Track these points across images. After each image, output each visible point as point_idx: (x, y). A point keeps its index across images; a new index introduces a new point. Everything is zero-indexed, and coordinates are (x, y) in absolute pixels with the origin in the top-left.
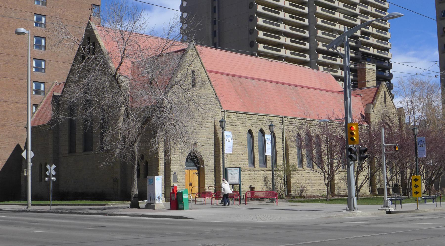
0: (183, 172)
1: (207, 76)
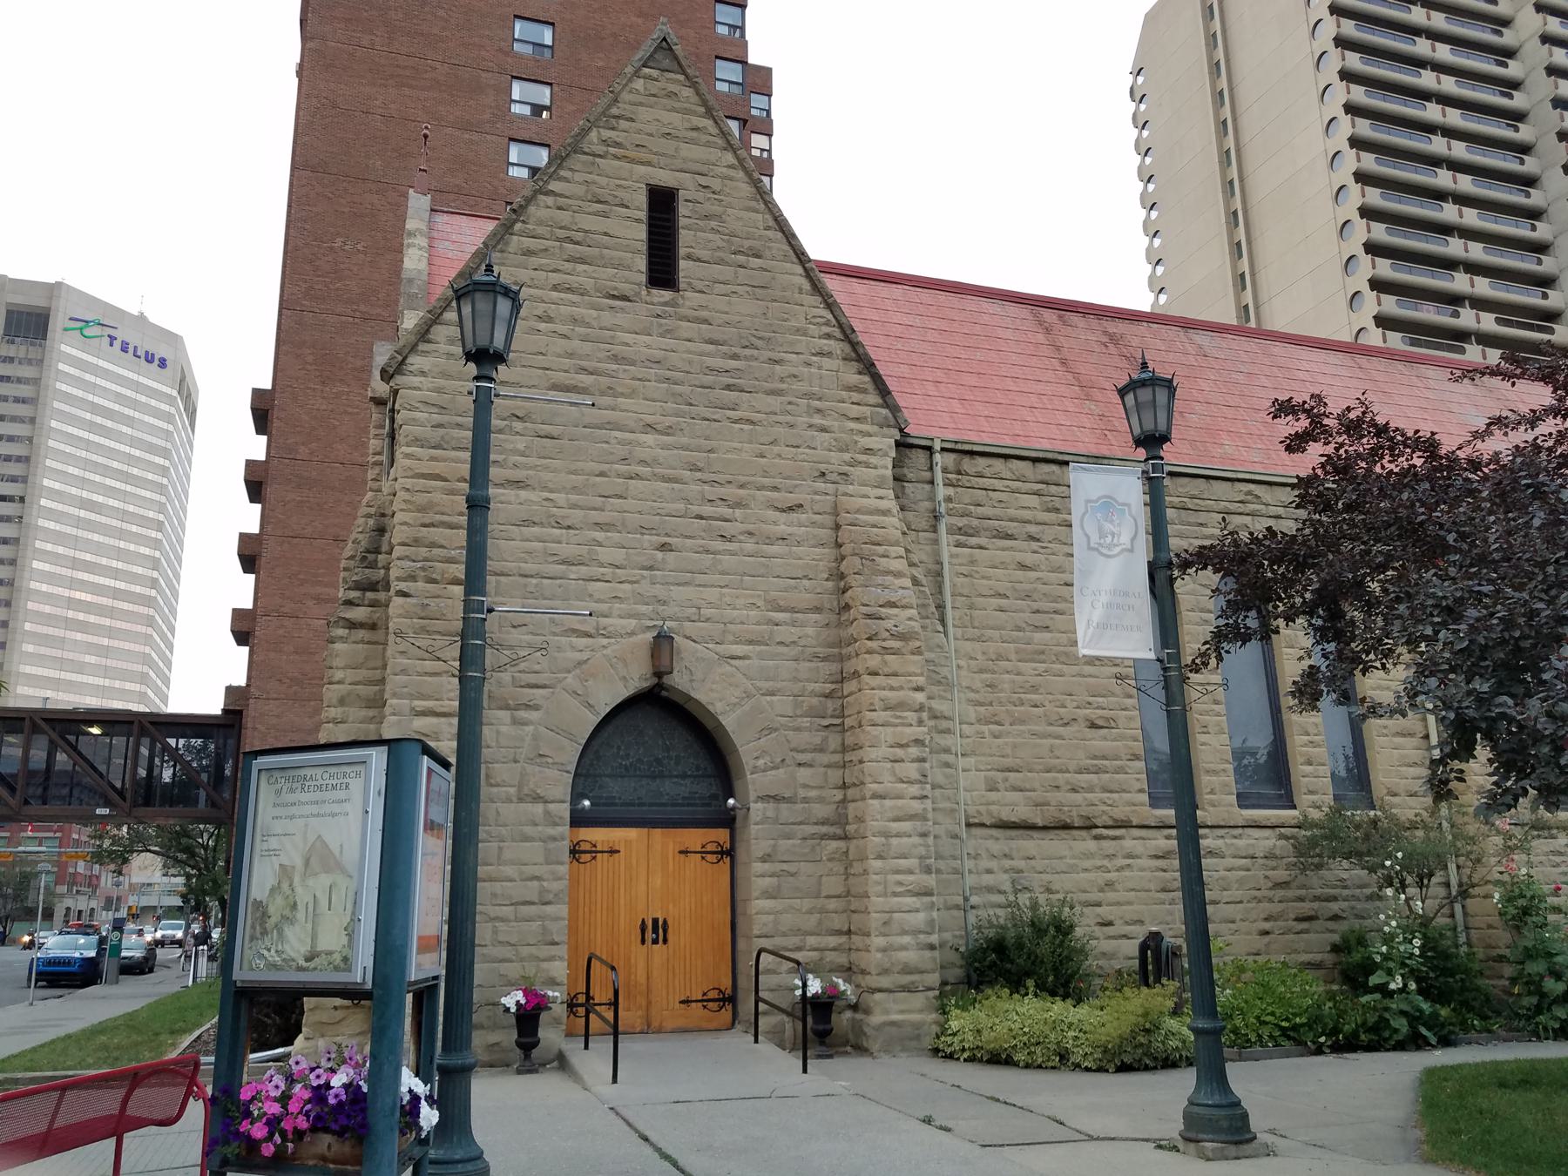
1: (771, 223)
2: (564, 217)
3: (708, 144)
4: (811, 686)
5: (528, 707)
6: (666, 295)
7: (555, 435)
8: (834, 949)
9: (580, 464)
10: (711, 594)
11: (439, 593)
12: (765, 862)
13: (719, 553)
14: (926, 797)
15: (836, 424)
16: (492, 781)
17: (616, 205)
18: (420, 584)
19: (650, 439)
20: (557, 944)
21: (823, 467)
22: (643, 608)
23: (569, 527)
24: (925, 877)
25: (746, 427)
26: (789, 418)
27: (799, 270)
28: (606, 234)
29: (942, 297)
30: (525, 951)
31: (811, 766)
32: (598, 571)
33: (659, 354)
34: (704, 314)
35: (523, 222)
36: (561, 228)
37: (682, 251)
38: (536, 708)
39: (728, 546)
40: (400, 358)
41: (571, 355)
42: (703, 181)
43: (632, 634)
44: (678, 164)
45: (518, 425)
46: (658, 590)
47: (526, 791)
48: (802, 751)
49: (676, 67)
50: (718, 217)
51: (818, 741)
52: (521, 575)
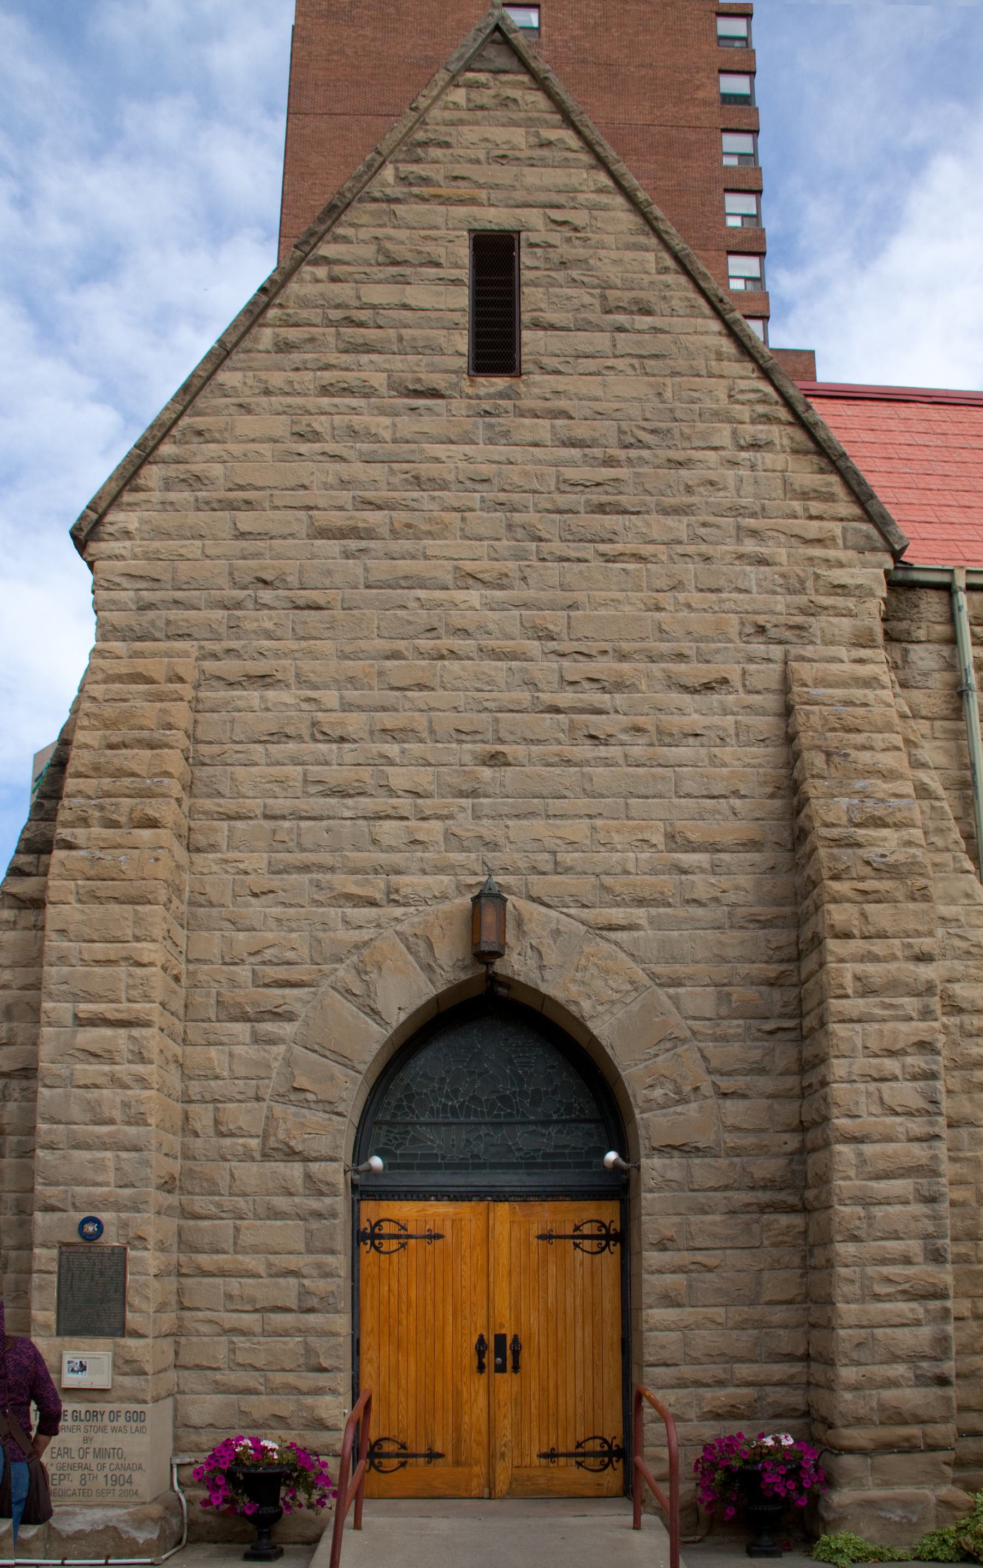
0: (315, 1225)
1: (670, 262)
2: (344, 292)
3: (565, 164)
4: (744, 969)
5: (277, 1016)
6: (500, 383)
7: (322, 602)
8: (781, 1383)
9: (363, 644)
10: (577, 829)
11: (119, 840)
12: (665, 1249)
13: (587, 763)
14: (937, 1137)
15: (783, 551)
16: (223, 1129)
17: (422, 265)
18: (96, 831)
19: (474, 596)
20: (324, 1370)
21: (761, 619)
22: (457, 857)
23: (342, 740)
24: (931, 1268)
25: (631, 567)
26: (704, 548)
27: (715, 326)
28: (405, 307)
29: (933, 412)
30: (278, 1378)
31: (744, 1096)
32: (382, 803)
33: (486, 470)
34: (562, 404)
35: (281, 306)
36: (338, 307)
37: (526, 317)
38: (289, 1017)
39: (602, 751)
40: (94, 516)
41: (344, 484)
42: (557, 215)
43: (444, 897)
44: (519, 196)
45: (266, 595)
46: (487, 828)
47: (272, 1143)
48: (729, 1074)
49: (513, 64)
50: (581, 262)
51: (756, 1054)
52: (266, 817)
